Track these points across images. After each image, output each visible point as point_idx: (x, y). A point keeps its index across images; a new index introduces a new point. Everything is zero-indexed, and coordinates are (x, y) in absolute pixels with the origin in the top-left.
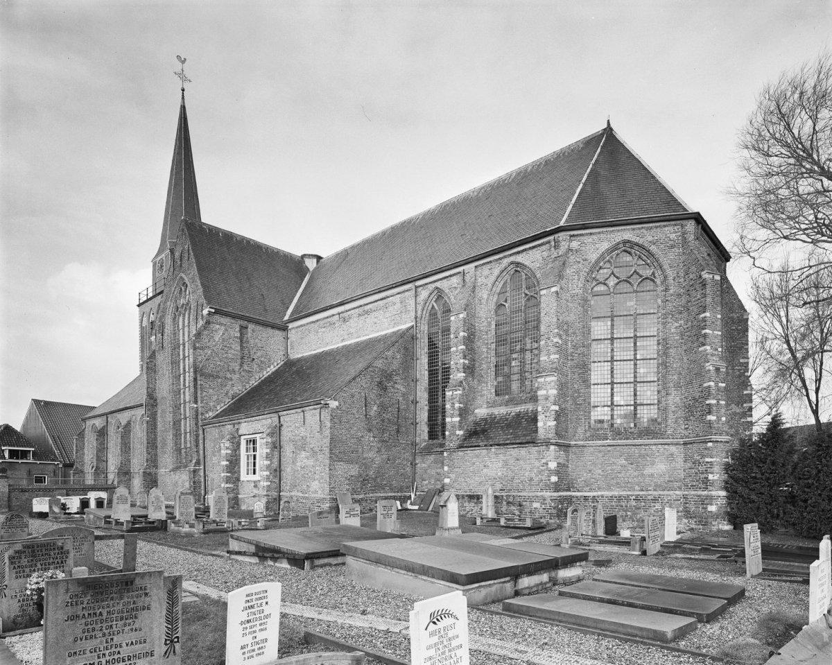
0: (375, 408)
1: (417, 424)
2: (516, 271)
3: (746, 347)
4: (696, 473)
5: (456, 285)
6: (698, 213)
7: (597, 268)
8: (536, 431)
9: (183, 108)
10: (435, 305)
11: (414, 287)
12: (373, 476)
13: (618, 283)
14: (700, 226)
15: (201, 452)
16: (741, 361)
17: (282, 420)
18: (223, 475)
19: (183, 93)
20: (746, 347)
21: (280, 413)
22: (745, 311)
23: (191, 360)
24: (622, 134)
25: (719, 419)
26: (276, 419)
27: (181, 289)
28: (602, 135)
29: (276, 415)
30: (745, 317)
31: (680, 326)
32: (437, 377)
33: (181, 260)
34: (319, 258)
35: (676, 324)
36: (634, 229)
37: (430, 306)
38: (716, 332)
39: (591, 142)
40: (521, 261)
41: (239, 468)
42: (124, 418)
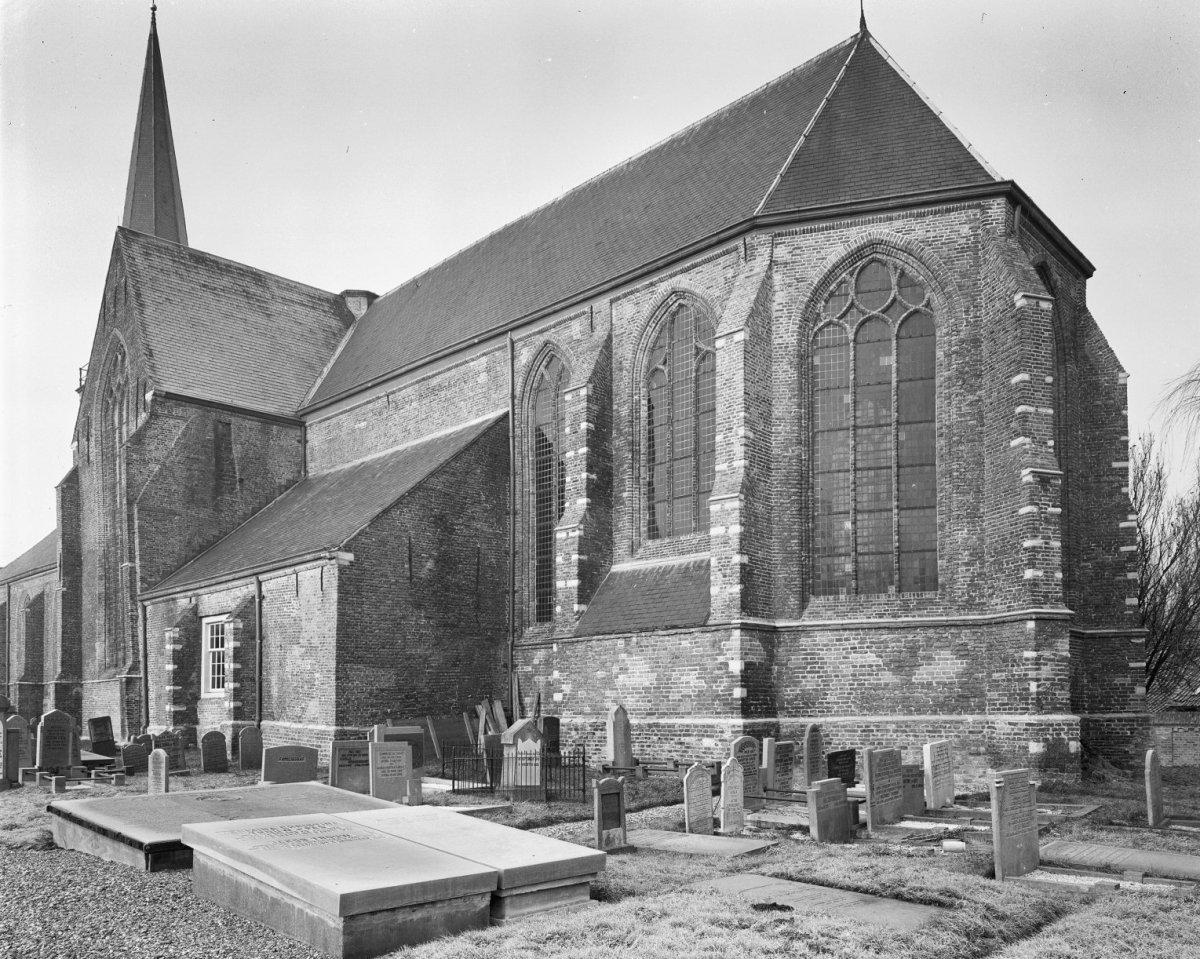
0: (430, 564)
1: (514, 592)
2: (681, 306)
3: (1123, 438)
4: (1009, 680)
5: (579, 336)
6: (1012, 183)
7: (826, 295)
8: (1130, 597)
9: (154, 39)
10: (545, 373)
11: (508, 342)
12: (426, 690)
13: (863, 323)
14: (1019, 209)
15: (141, 647)
16: (1115, 465)
17: (264, 589)
18: (168, 688)
19: (154, 14)
20: (1123, 438)
21: (261, 577)
22: (1121, 369)
23: (124, 482)
24: (885, 41)
25: (1049, 574)
26: (253, 588)
27: (117, 357)
28: (851, 46)
29: (254, 579)
30: (1121, 381)
31: (979, 401)
32: (550, 506)
33: (115, 306)
34: (371, 297)
35: (971, 398)
36: (891, 219)
37: (538, 377)
38: (1042, 410)
39: (828, 61)
40: (688, 287)
41: (199, 676)
42: (32, 588)
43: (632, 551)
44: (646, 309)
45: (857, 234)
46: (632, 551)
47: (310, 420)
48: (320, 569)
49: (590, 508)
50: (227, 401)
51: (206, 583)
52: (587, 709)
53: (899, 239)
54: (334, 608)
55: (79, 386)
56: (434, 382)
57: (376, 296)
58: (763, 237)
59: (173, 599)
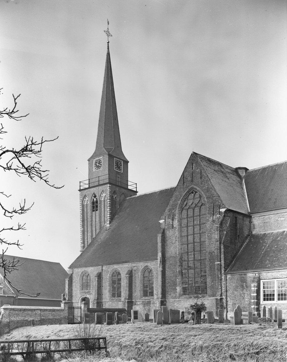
9: (108, 54)
19: (108, 45)
34: (246, 169)
45: (83, 269)
49: (115, 215)
50: (237, 210)
51: (252, 271)
55: (79, 189)
57: (248, 170)
59: (245, 274)
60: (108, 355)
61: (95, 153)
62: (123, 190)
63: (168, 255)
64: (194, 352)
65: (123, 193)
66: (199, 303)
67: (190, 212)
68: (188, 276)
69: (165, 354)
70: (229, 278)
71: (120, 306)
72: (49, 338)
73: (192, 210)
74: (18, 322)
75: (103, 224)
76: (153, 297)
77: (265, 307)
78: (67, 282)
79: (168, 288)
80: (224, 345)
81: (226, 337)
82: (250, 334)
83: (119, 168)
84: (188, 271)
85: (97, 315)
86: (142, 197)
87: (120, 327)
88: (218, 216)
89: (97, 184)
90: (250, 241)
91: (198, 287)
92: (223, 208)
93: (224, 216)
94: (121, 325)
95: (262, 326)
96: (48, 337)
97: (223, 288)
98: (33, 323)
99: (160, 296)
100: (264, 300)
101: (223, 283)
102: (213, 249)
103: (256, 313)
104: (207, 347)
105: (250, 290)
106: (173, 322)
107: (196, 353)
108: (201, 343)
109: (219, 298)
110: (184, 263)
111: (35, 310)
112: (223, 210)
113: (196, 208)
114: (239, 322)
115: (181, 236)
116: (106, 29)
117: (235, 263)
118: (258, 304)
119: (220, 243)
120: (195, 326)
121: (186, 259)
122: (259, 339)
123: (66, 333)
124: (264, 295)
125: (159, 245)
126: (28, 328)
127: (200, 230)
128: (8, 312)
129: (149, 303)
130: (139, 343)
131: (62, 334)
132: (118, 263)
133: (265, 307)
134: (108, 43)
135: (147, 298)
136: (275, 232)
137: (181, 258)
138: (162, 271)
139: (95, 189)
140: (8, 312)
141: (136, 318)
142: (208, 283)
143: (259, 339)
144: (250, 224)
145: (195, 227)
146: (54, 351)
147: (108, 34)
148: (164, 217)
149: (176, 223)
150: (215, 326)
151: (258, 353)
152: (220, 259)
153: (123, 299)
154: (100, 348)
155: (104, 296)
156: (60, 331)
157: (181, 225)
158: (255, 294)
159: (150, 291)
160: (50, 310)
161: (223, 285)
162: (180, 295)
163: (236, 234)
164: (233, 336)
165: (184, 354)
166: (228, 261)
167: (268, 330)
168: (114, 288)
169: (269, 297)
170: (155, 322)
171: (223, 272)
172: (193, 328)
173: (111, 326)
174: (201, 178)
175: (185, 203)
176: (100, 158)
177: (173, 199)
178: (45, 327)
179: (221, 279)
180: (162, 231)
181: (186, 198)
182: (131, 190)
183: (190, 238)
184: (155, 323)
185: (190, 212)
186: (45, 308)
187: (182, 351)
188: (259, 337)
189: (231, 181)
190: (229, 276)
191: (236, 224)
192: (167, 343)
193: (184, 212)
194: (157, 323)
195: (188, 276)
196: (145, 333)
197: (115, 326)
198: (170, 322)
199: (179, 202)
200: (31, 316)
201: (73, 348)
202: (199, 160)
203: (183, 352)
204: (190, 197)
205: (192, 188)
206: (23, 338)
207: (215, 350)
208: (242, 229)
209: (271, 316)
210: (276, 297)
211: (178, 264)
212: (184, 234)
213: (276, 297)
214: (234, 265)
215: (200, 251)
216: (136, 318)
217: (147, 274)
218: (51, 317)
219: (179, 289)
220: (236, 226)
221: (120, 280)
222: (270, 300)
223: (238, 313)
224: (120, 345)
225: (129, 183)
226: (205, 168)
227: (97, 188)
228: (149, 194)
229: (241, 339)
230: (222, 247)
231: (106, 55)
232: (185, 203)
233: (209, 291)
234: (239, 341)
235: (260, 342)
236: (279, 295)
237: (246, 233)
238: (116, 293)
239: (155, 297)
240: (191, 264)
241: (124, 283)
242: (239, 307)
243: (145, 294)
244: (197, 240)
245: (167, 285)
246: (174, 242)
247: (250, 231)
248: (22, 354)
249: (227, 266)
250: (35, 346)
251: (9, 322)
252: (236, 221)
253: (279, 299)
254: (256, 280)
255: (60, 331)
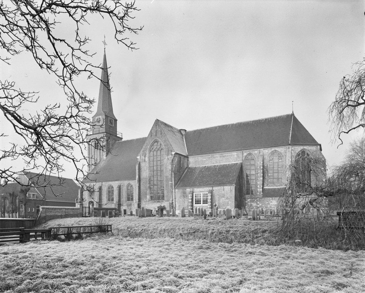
34: (185, 131)
43: (267, 185)
44: (270, 152)
45: (302, 147)
46: (267, 185)
47: (189, 157)
48: (13, 173)
50: (181, 153)
52: (265, 208)
53: (307, 149)
54: (234, 193)
56: (224, 155)
58: (290, 146)
60: (113, 235)
61: (96, 113)
62: (114, 137)
63: (142, 177)
64: (161, 233)
65: (114, 139)
66: (162, 205)
67: (155, 153)
68: (154, 190)
69: (145, 234)
70: (177, 191)
71: (113, 206)
72: (73, 226)
73: (156, 152)
74: (51, 216)
75: (101, 157)
76: (133, 201)
77: (196, 208)
78: (79, 191)
79: (142, 196)
80: (177, 228)
81: (177, 224)
82: (190, 222)
83: (112, 123)
84: (154, 186)
85: (102, 212)
86: (125, 142)
87: (117, 219)
88: (171, 156)
89: (98, 132)
90: (188, 171)
91: (159, 196)
92: (173, 152)
93: (174, 156)
94: (117, 218)
95: (196, 218)
96: (72, 225)
97: (173, 197)
98: (61, 217)
99: (138, 201)
100: (196, 204)
101: (174, 194)
102: (168, 175)
103: (191, 211)
104: (168, 230)
105: (188, 198)
106: (147, 216)
107: (162, 233)
108: (164, 227)
109: (171, 202)
110: (151, 182)
111: (62, 209)
112: (173, 153)
113: (158, 151)
114: (184, 216)
115: (150, 167)
116: (103, 41)
117: (180, 183)
118: (192, 206)
119: (172, 172)
120: (160, 218)
121: (152, 179)
122: (195, 225)
123: (84, 223)
124: (196, 201)
125: (137, 171)
126: (58, 220)
127: (160, 163)
128: (44, 210)
129: (131, 205)
130: (129, 228)
131: (81, 223)
132: (112, 181)
133: (196, 208)
134: (105, 48)
135: (129, 202)
136: (201, 166)
137: (150, 179)
138: (139, 186)
139: (97, 135)
140: (44, 210)
141: (125, 213)
142: (165, 194)
143: (195, 225)
144: (188, 161)
145: (158, 161)
146: (83, 233)
147: (105, 43)
148: (140, 155)
149: (147, 159)
150: (171, 218)
151: (194, 232)
152: (172, 180)
153: (115, 202)
154: (108, 231)
155: (103, 201)
156: (80, 221)
157: (149, 160)
158: (191, 201)
159: (131, 198)
160: (71, 209)
161: (173, 195)
162: (149, 200)
163: (180, 166)
164: (181, 224)
165: (155, 234)
166: (176, 182)
167: (199, 220)
168: (109, 196)
169: (198, 202)
170: (137, 216)
171: (173, 188)
172: (159, 219)
173: (111, 219)
174: (161, 134)
175: (152, 148)
176: (100, 117)
177: (145, 145)
178: (69, 219)
179: (172, 192)
180: (138, 163)
181: (152, 145)
182: (118, 137)
183: (155, 168)
184: (137, 217)
185: (155, 153)
186: (68, 207)
187: (154, 232)
188: (195, 224)
189: (178, 137)
190: (176, 190)
191: (180, 161)
192: (145, 228)
193: (152, 153)
194: (138, 217)
195: (154, 190)
196: (132, 222)
197: (113, 218)
198: (145, 216)
199: (149, 147)
200: (59, 212)
201: (93, 231)
202: (160, 124)
203: (155, 233)
204: (154, 144)
205: (156, 139)
206: (55, 226)
207: (172, 231)
208: (183, 164)
209: (200, 213)
210: (202, 202)
211: (148, 182)
212: (159, 162)
213: (202, 202)
214: (179, 184)
215: (161, 175)
216: (125, 213)
217: (129, 188)
218: (72, 213)
219: (148, 197)
220: (180, 162)
221: (113, 191)
222: (199, 204)
223: (183, 211)
224: (118, 229)
225: (118, 133)
226: (163, 129)
227: (98, 135)
228: (130, 140)
229: (185, 225)
230: (173, 173)
231: (103, 56)
232: (152, 148)
233: (165, 198)
234: (184, 226)
235: (195, 226)
236: (203, 201)
237: (186, 166)
238: (110, 199)
239: (134, 201)
240: (155, 183)
241: (116, 193)
242: (183, 208)
243: (128, 200)
244: (159, 169)
245: (142, 194)
246: (145, 170)
247: (188, 165)
248: (64, 235)
249: (175, 184)
250: (72, 230)
251: (45, 216)
252: (180, 159)
253: (203, 203)
254: (191, 193)
255: (80, 221)
